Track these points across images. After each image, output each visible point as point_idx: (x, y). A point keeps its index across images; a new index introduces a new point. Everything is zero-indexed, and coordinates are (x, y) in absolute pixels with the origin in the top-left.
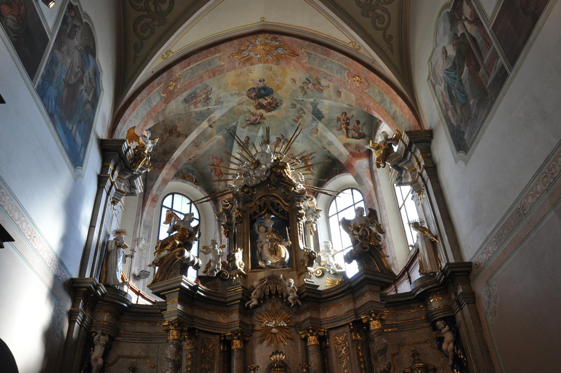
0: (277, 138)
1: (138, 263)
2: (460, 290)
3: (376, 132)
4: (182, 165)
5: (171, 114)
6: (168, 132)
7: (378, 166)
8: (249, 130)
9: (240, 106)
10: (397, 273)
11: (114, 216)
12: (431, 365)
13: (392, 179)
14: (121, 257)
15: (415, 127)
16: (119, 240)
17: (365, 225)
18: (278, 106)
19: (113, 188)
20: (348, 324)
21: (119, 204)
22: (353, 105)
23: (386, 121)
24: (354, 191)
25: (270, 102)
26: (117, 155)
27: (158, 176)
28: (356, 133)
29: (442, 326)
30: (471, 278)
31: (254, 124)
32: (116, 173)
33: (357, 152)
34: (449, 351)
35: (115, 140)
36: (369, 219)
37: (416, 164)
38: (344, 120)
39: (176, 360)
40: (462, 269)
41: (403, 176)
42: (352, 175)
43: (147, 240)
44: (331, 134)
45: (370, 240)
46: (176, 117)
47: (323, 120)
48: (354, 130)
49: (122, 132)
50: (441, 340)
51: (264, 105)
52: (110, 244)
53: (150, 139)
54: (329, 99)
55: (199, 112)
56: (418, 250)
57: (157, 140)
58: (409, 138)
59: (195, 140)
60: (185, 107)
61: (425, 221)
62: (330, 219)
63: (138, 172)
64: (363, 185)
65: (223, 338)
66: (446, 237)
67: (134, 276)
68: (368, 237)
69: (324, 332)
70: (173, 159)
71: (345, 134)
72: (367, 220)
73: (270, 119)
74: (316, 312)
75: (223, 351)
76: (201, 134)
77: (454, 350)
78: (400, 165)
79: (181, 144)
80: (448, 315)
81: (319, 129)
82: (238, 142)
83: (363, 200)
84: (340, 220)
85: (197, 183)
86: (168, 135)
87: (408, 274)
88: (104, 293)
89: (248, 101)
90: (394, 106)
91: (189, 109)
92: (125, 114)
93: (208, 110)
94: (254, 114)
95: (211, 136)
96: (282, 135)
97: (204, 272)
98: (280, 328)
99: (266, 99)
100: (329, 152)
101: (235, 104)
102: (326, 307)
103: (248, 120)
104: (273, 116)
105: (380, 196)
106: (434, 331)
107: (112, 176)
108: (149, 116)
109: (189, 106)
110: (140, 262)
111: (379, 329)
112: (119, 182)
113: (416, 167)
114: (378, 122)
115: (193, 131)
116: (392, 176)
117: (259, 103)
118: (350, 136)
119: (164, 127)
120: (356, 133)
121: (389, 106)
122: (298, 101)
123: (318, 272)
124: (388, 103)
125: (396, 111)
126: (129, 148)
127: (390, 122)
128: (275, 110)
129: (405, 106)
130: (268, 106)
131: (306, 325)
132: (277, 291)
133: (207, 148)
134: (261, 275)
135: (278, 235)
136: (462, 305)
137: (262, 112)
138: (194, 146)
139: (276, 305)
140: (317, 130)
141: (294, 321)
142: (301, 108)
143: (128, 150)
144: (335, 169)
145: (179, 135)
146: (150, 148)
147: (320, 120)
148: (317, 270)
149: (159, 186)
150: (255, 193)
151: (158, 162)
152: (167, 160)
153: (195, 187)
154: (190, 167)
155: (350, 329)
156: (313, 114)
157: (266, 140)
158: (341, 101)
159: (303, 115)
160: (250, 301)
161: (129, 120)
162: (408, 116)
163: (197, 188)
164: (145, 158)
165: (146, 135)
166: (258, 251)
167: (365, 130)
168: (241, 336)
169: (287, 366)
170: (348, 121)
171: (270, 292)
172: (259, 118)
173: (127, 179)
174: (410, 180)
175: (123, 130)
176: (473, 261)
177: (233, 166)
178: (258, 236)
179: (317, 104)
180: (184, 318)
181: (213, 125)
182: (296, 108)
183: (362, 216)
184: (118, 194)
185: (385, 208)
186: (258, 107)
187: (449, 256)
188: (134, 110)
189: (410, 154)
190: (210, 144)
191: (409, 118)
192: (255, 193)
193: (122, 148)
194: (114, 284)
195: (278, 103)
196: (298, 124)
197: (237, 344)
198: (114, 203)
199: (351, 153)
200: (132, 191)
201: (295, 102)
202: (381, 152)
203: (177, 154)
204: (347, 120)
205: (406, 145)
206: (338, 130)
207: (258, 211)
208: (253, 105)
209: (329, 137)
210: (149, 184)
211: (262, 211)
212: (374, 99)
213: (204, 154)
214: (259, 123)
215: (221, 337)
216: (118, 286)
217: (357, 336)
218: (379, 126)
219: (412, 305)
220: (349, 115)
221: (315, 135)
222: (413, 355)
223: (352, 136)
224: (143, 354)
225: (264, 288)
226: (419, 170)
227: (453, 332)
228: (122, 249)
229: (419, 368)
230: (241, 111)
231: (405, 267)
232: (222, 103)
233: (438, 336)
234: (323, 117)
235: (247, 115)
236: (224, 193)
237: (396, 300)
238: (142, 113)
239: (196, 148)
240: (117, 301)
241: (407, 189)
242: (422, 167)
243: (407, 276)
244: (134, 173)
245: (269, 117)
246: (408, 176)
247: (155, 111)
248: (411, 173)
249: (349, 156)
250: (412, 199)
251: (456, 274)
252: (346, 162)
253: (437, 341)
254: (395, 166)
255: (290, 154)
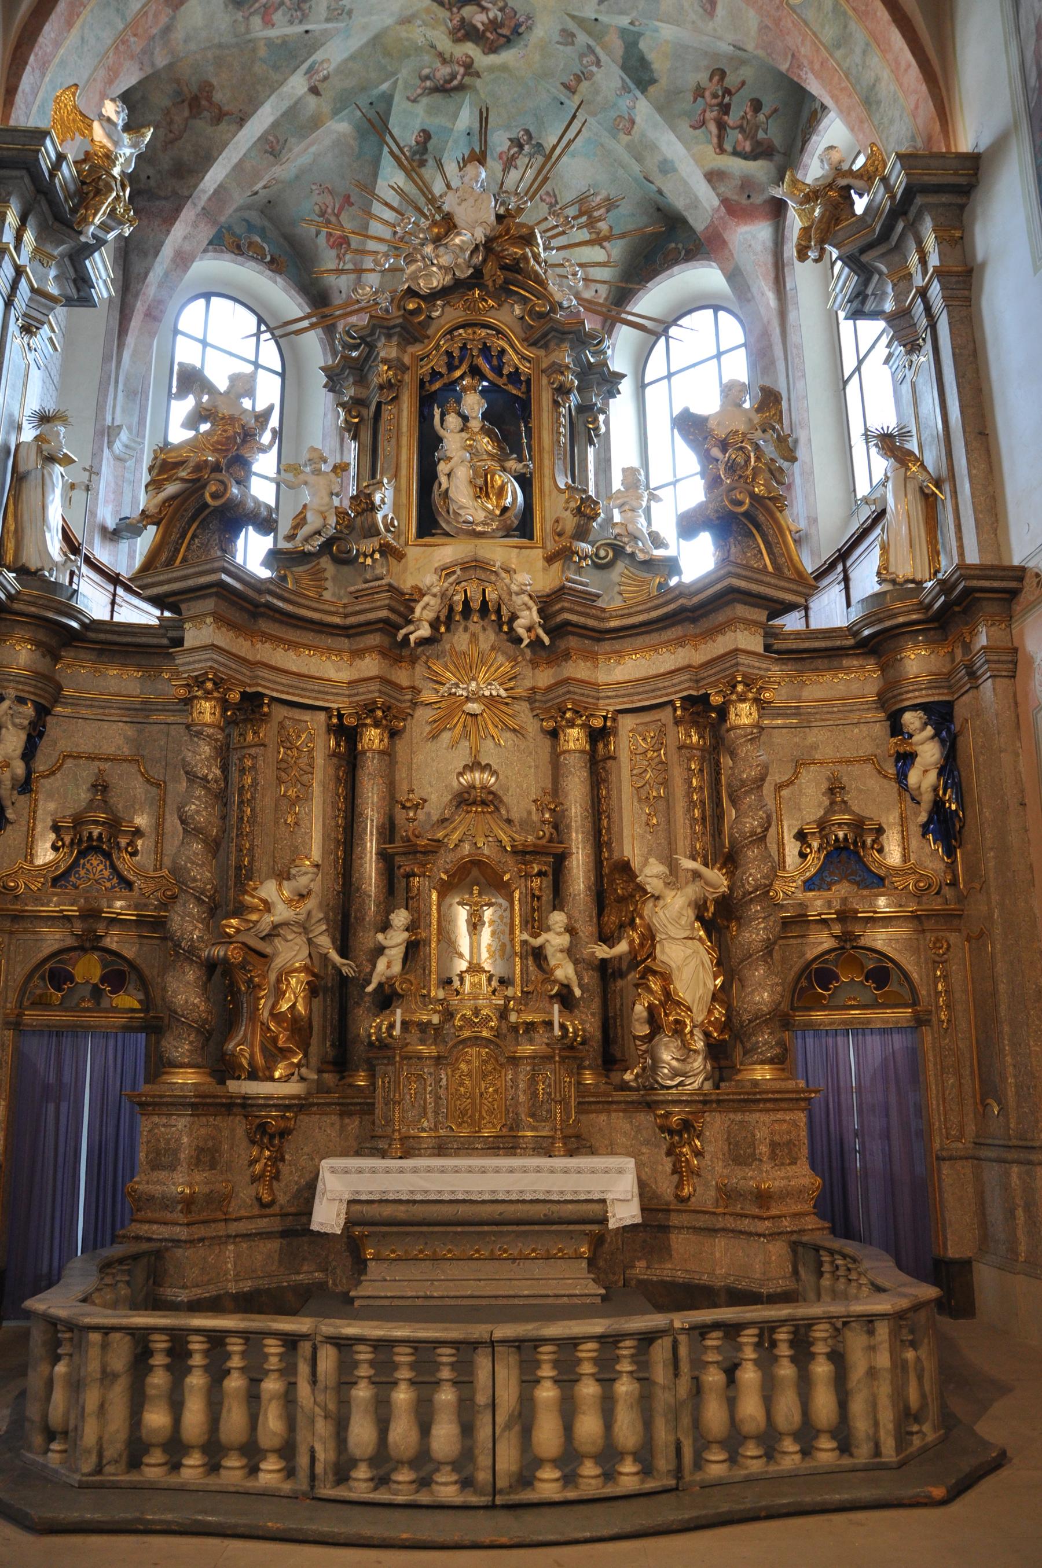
0: (510, 140)
1: (112, 496)
2: (982, 640)
3: (805, 141)
4: (231, 211)
5: (193, 46)
6: (186, 104)
7: (802, 256)
8: (431, 111)
9: (404, 27)
10: (809, 565)
11: (33, 366)
12: (872, 819)
13: (836, 298)
14: (58, 491)
15: (930, 138)
16: (49, 442)
17: (744, 434)
18: (520, 34)
19: (23, 284)
20: (671, 703)
21: (45, 332)
22: (750, 47)
23: (841, 111)
24: (722, 314)
25: (496, 18)
26: (27, 180)
27: (162, 243)
28: (746, 139)
29: (917, 724)
30: (1017, 608)
31: (446, 89)
32: (29, 237)
33: (744, 201)
34: (923, 789)
35: (15, 130)
36: (757, 419)
37: (914, 259)
38: (715, 96)
39: (210, 777)
40: (996, 584)
41: (869, 291)
42: (722, 270)
43: (135, 431)
44: (673, 137)
45: (753, 480)
46: (209, 55)
47: (651, 89)
48: (741, 128)
49: (38, 102)
50: (906, 759)
51: (475, 28)
52: (23, 451)
53: (127, 128)
54: (677, 23)
55: (279, 41)
56: (883, 512)
57: (149, 134)
58: (907, 174)
59: (266, 133)
60: (235, 21)
61: (914, 432)
62: (648, 391)
63: (94, 236)
64: (749, 301)
65: (335, 721)
66: (967, 486)
67: (104, 529)
68: (749, 472)
69: (605, 718)
70: (204, 191)
71: (715, 140)
72: (750, 420)
73: (493, 76)
74: (589, 664)
75: (334, 754)
76: (284, 115)
77: (935, 789)
78: (865, 258)
79: (225, 145)
80: (936, 699)
81: (638, 120)
82: (392, 153)
83: (744, 345)
84: (676, 412)
85: (275, 265)
86: (186, 113)
87: (845, 571)
88: (13, 592)
89: (427, 10)
90: (875, 61)
91: (248, 31)
92: (41, 39)
93: (307, 36)
94: (447, 56)
95: (315, 123)
96: (527, 132)
97: (290, 538)
98: (492, 701)
99: (484, 9)
100: (660, 192)
101: (389, 21)
102: (615, 652)
103: (427, 78)
104: (504, 68)
105: (792, 338)
106: (893, 735)
107: (17, 248)
108: (122, 48)
109: (247, 19)
110: (119, 492)
111: (752, 726)
112: (40, 268)
113: (913, 270)
114: (816, 110)
115: (263, 103)
116: (838, 290)
117: (463, 20)
118: (728, 147)
119: (175, 86)
120: (746, 139)
121: (858, 60)
122: (580, 22)
123: (602, 553)
124: (858, 50)
125: (877, 79)
126: (61, 157)
127: (853, 114)
128: (509, 48)
129: (909, 66)
130: (488, 34)
131: (559, 696)
132: (484, 603)
133: (305, 160)
134: (448, 552)
135: (498, 441)
136: (978, 678)
137: (471, 53)
138: (266, 152)
139: (482, 637)
140: (633, 122)
141: (528, 684)
142: (589, 46)
143: (57, 166)
144: (673, 245)
145: (220, 116)
146: (128, 160)
147: (644, 91)
148: (598, 549)
149: (166, 274)
150: (437, 314)
151: (159, 198)
152: (186, 194)
153: (270, 279)
154: (254, 216)
155: (675, 718)
156: (624, 68)
157: (477, 150)
158: (715, 30)
159: (594, 69)
160: (411, 628)
161: (57, 60)
162: (912, 100)
163: (275, 282)
164: (114, 194)
165: (114, 117)
166: (440, 484)
167: (773, 133)
168: (385, 717)
169: (501, 801)
170: (727, 99)
171: (466, 603)
172: (462, 70)
173: (62, 256)
174: (889, 306)
175: (40, 95)
176: (1031, 565)
177: (376, 228)
178: (440, 440)
179: (640, 35)
180: (231, 668)
181: (320, 86)
182: (573, 44)
183: (740, 406)
184: (38, 302)
185: (804, 376)
186: (460, 34)
187: (966, 541)
188: (70, 24)
189: (900, 226)
190: (313, 149)
191: (917, 107)
192: (437, 314)
193: (38, 160)
194: (39, 566)
195: (520, 25)
196: (577, 99)
197: (372, 737)
198: (27, 330)
199: (725, 202)
200: (82, 294)
201: (572, 26)
202: (817, 213)
203: (215, 176)
204: (723, 97)
205: (893, 197)
206: (694, 128)
207: (443, 370)
208: (443, 28)
209: (664, 148)
210: (137, 267)
211: (457, 368)
212: (815, 34)
213: (297, 177)
214: (461, 88)
215: (330, 718)
216: (51, 570)
217: (690, 736)
218: (819, 122)
219: (845, 662)
220: (731, 81)
221: (625, 138)
222: (831, 791)
223: (734, 148)
224: (126, 751)
225: (451, 592)
226: (919, 281)
227: (943, 742)
228: (58, 469)
229: (840, 824)
230: (406, 43)
231: (839, 550)
232: (350, 13)
233: (901, 750)
234: (653, 81)
235: (426, 58)
236: (352, 307)
237: (807, 645)
238: (98, 39)
239: (271, 158)
240: (50, 615)
241: (872, 329)
242: (931, 270)
243: (841, 576)
244: (83, 239)
245: (491, 69)
246: (884, 293)
247: (140, 31)
248: (894, 285)
249: (718, 210)
250: (887, 361)
251: (978, 595)
252: (707, 228)
253: (897, 761)
254: (851, 261)
255: (548, 193)
